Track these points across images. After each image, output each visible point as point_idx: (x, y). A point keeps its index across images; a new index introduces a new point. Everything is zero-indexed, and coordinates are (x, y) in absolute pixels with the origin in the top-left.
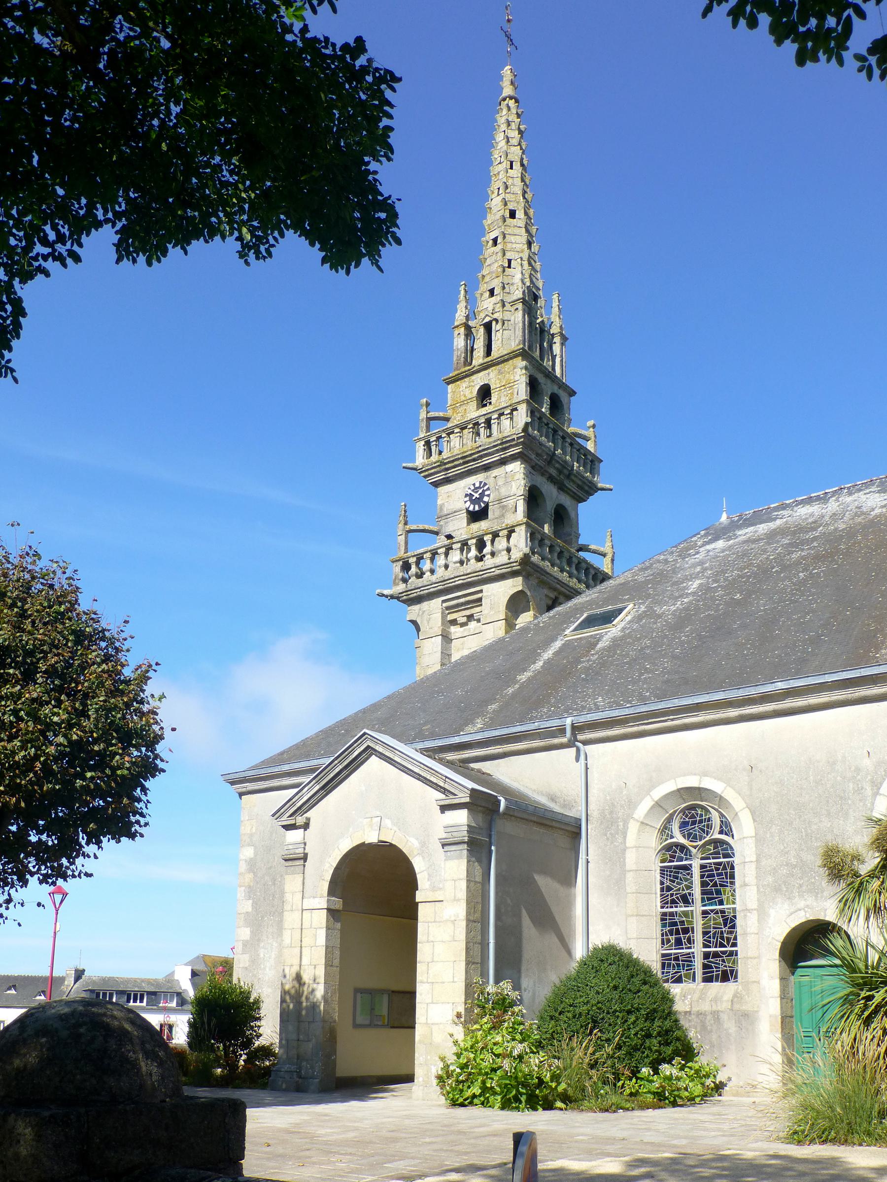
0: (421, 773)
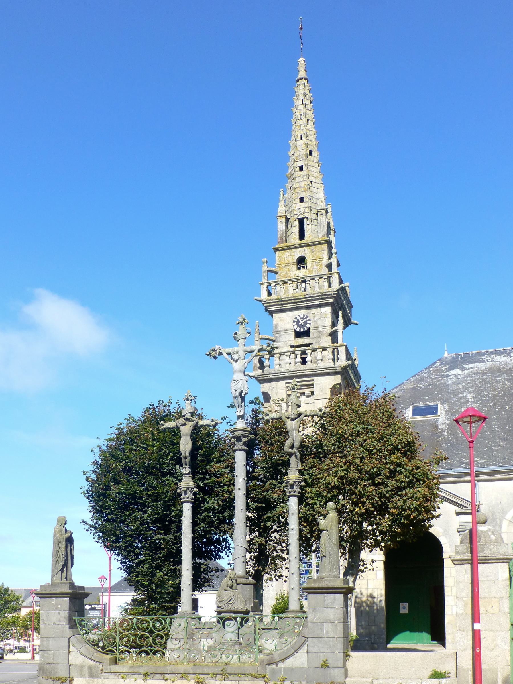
0: (446, 496)
